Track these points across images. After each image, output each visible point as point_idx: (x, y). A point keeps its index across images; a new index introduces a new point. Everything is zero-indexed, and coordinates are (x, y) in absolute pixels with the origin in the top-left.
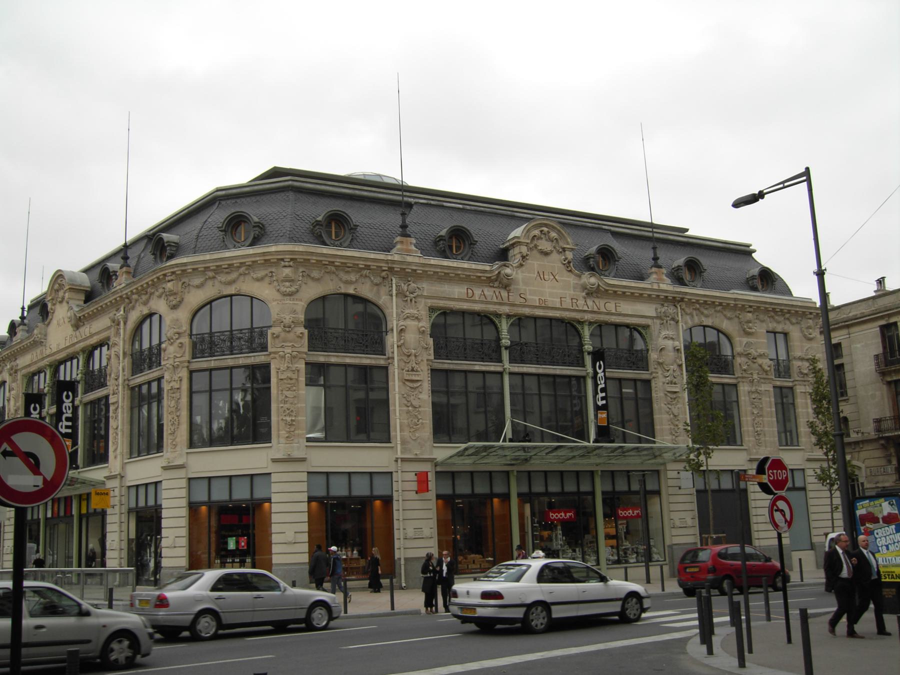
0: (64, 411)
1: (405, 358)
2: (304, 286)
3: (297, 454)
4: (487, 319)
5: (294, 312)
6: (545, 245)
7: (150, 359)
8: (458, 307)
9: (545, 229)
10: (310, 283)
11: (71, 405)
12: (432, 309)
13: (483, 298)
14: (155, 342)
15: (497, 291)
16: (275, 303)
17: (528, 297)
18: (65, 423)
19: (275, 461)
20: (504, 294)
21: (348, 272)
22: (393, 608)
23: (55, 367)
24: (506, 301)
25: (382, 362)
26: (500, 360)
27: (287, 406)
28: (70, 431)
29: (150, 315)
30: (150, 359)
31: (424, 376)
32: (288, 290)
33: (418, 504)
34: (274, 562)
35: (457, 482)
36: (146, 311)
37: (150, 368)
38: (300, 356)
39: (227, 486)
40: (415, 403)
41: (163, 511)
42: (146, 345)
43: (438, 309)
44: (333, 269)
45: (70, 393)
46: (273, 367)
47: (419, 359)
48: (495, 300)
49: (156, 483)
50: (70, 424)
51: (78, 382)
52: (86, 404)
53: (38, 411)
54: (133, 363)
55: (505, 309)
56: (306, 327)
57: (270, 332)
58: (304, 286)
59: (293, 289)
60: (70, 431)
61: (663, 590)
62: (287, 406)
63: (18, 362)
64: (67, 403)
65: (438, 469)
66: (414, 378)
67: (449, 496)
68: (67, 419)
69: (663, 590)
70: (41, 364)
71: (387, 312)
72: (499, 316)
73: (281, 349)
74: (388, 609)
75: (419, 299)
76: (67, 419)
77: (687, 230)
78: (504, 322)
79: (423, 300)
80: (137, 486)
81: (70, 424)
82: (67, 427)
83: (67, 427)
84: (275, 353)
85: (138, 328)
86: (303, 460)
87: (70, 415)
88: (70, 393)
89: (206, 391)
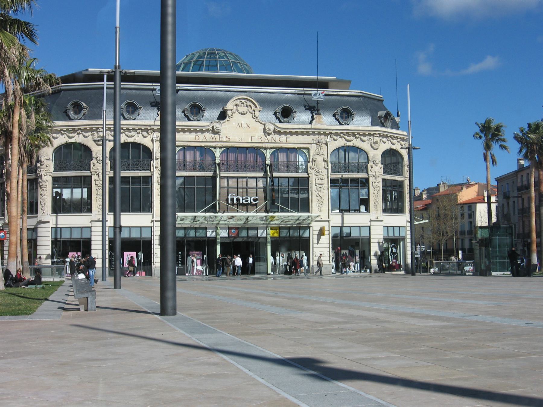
4: (204, 150)
9: (243, 101)
20: (217, 136)
24: (218, 140)
25: (86, 173)
41: (92, 251)
72: (266, 149)
86: (382, 221)
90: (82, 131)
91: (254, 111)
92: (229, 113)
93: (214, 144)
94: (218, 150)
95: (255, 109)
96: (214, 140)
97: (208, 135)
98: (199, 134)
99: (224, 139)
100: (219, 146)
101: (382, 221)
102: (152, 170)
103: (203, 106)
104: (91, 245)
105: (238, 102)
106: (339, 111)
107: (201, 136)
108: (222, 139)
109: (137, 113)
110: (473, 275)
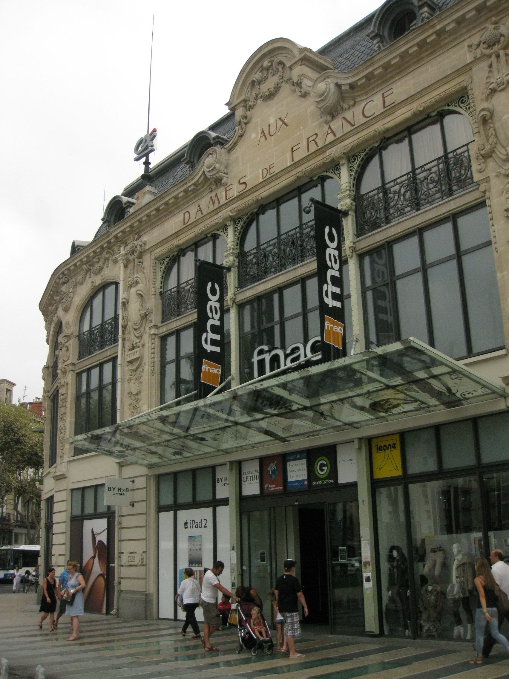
0: (210, 315)
7: (102, 337)
11: (218, 305)
14: (109, 314)
20: (221, 192)
23: (248, 220)
28: (217, 349)
29: (104, 287)
30: (102, 337)
36: (98, 280)
37: (102, 346)
39: (142, 487)
42: (97, 321)
45: (217, 286)
49: (96, 487)
50: (217, 337)
51: (229, 269)
52: (241, 307)
53: (217, 297)
54: (80, 346)
60: (217, 349)
63: (145, 238)
64: (213, 302)
68: (214, 329)
70: (335, 152)
80: (83, 489)
81: (217, 337)
85: (89, 303)
87: (218, 323)
88: (217, 286)
89: (433, 265)
96: (217, 205)
99: (235, 190)
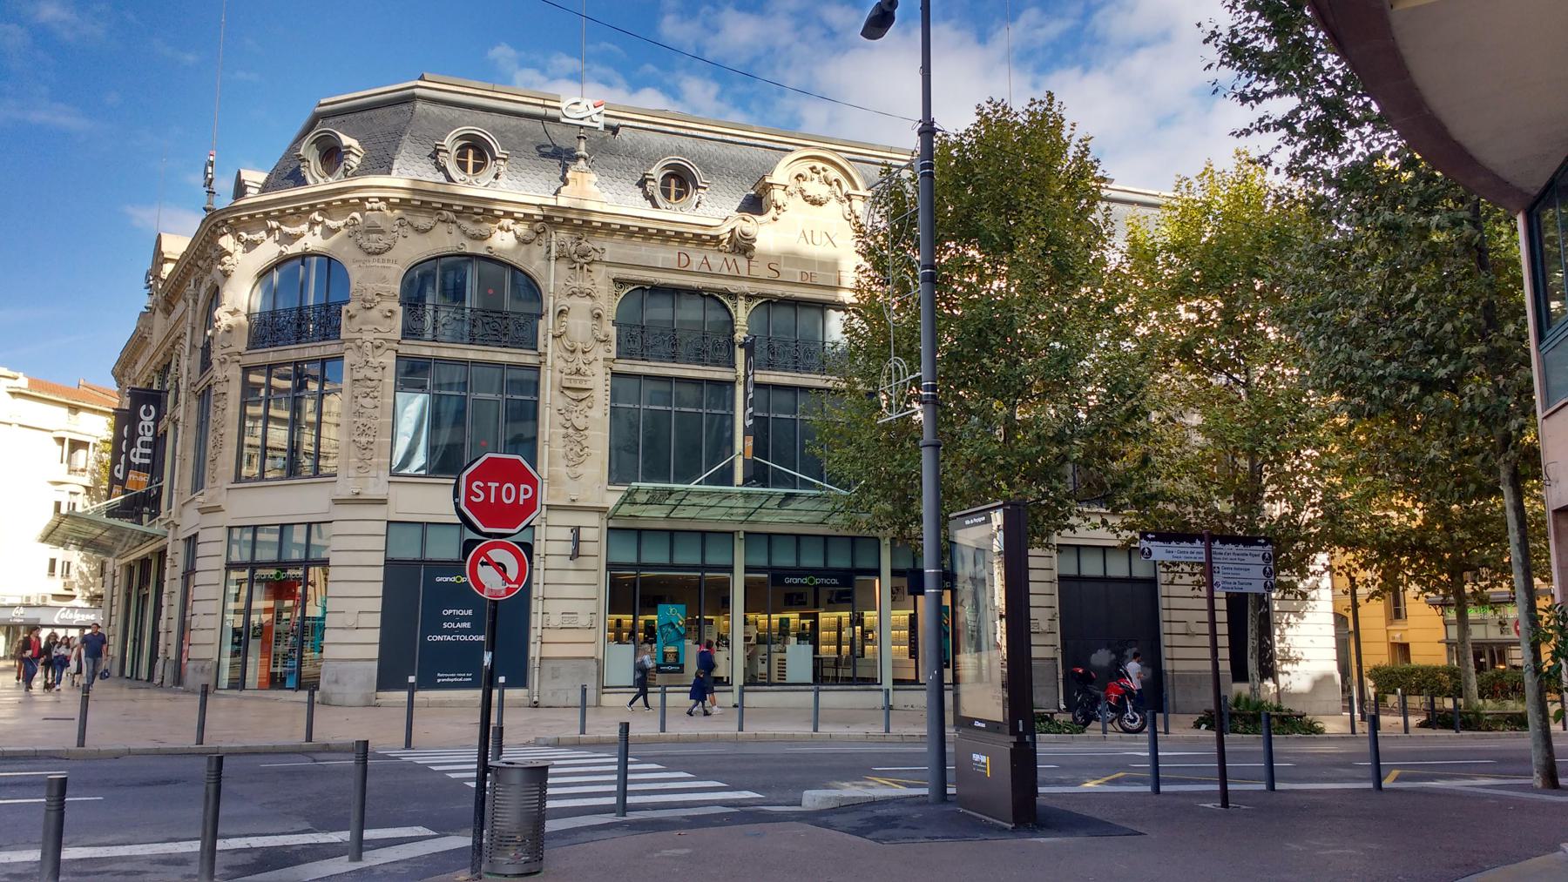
1: (566, 355)
2: (400, 240)
3: (372, 492)
5: (384, 279)
6: (815, 188)
8: (662, 281)
9: (819, 165)
10: (412, 235)
12: (620, 283)
13: (705, 269)
15: (730, 258)
16: (355, 266)
17: (783, 269)
18: (140, 450)
19: (337, 502)
20: (742, 262)
21: (477, 222)
22: (200, 741)
24: (744, 273)
25: (530, 359)
26: (732, 365)
27: (363, 420)
28: (147, 461)
31: (599, 383)
32: (374, 245)
33: (571, 577)
34: (1034, 655)
35: (644, 546)
38: (387, 345)
40: (580, 423)
43: (632, 282)
44: (452, 216)
46: (346, 361)
47: (590, 357)
48: (726, 272)
50: (148, 451)
55: (746, 287)
56: (402, 304)
57: (344, 308)
58: (400, 240)
59: (381, 245)
60: (147, 461)
61: (663, 730)
62: (363, 420)
65: (611, 524)
66: (578, 385)
67: (846, 570)
68: (144, 444)
69: (663, 730)
71: (542, 284)
72: (733, 296)
73: (358, 335)
74: (71, 744)
75: (594, 267)
76: (144, 444)
77: (1112, 181)
78: (741, 304)
79: (604, 268)
81: (148, 451)
82: (142, 455)
83: (142, 455)
84: (352, 340)
86: (383, 502)
90: (323, 212)
91: (848, 197)
92: (778, 195)
93: (732, 286)
94: (741, 304)
95: (851, 191)
97: (717, 261)
98: (689, 248)
100: (747, 290)
101: (383, 502)
102: (541, 349)
103: (701, 177)
104: (384, 597)
105: (804, 168)
106: (657, 172)
107: (697, 258)
108: (755, 272)
109: (695, 198)
110: (546, 768)
